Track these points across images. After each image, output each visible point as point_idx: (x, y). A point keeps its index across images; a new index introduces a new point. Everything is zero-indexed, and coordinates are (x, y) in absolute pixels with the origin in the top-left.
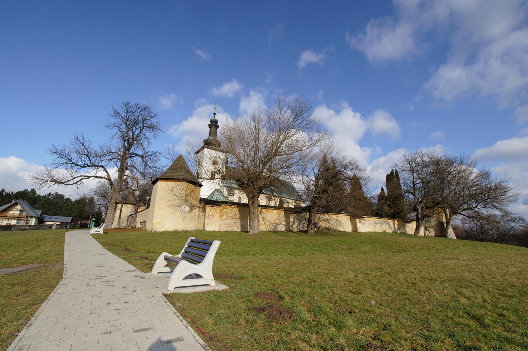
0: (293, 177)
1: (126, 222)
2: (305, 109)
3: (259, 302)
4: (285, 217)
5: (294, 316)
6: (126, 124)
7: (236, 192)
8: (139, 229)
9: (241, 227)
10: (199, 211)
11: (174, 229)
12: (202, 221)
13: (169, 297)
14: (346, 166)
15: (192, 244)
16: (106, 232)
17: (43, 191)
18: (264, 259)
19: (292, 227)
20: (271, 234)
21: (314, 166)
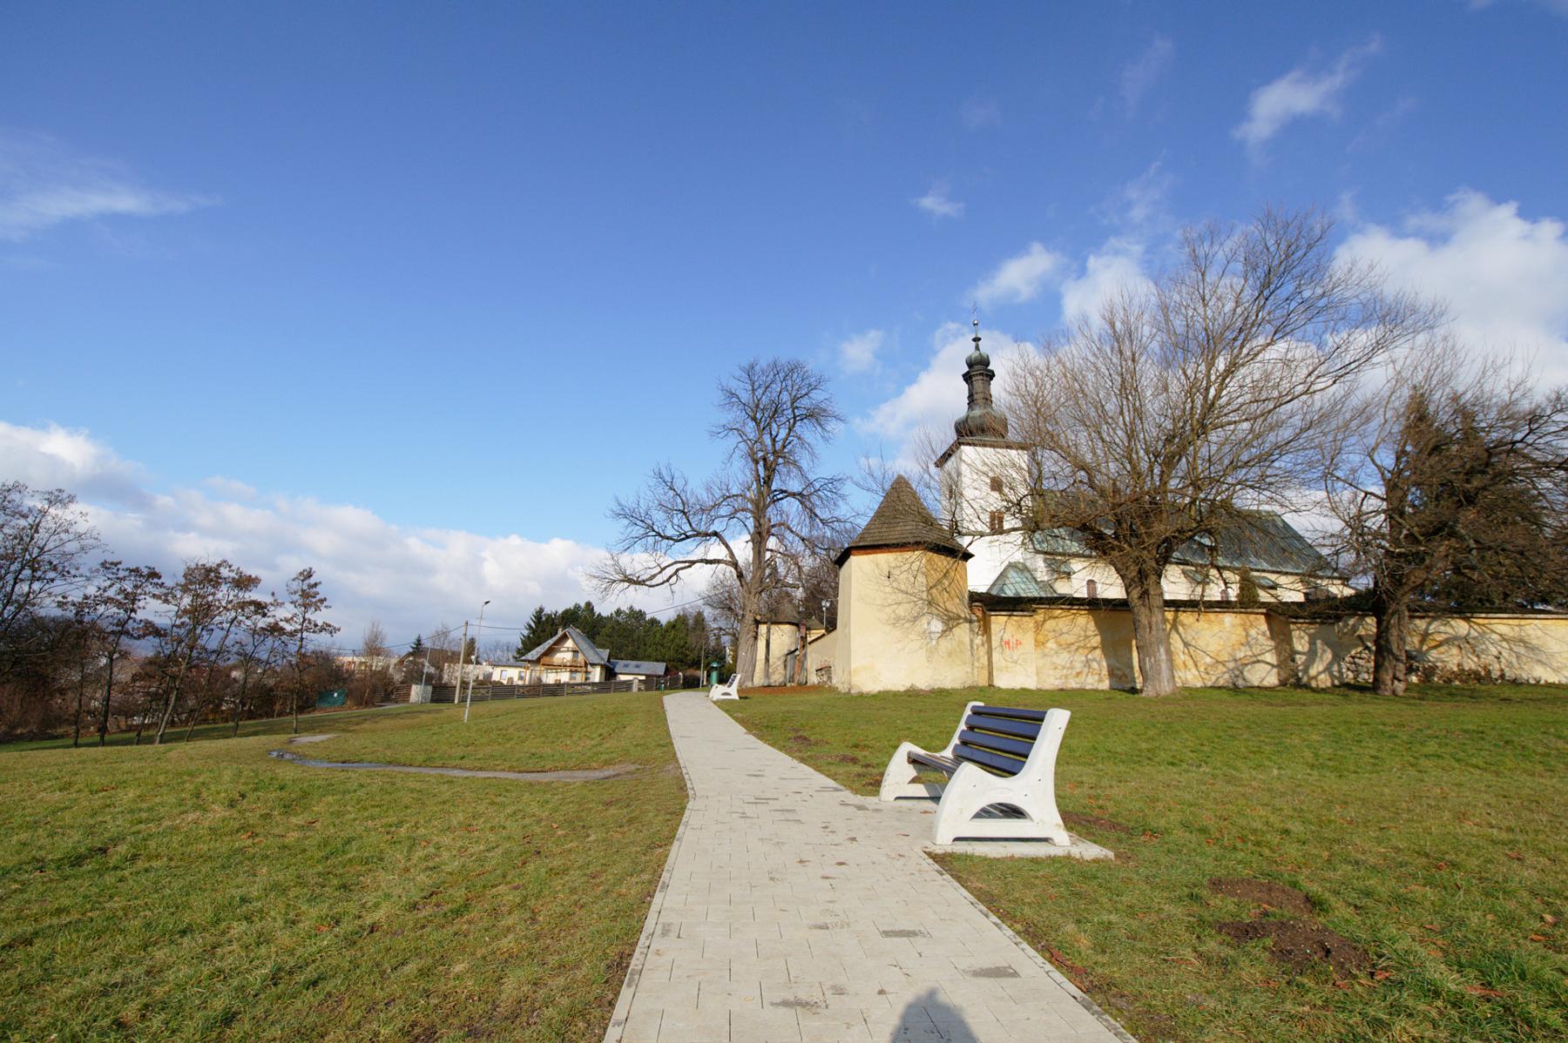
0: (1287, 493)
1: (781, 669)
2: (1303, 242)
3: (1232, 908)
4: (1272, 638)
5: (1385, 969)
6: (754, 419)
7: (1076, 565)
8: (817, 688)
9: (1111, 674)
10: (971, 630)
11: (908, 685)
12: (985, 660)
13: (944, 861)
14: (1534, 418)
15: (979, 721)
16: (744, 694)
17: (604, 609)
18: (1214, 776)
19: (1306, 671)
20: (1224, 695)
21: (1371, 441)
